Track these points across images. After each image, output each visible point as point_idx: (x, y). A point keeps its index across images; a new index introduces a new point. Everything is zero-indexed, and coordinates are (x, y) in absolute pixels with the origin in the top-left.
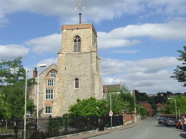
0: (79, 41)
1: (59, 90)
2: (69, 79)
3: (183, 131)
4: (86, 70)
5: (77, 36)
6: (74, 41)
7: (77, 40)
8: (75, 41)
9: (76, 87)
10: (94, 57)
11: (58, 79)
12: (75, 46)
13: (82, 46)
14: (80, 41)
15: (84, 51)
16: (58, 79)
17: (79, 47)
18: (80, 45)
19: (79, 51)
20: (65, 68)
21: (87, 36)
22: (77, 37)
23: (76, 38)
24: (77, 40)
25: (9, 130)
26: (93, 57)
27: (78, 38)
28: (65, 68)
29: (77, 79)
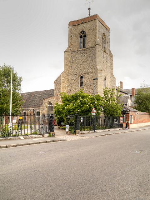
0: (85, 36)
1: (64, 89)
2: (74, 78)
3: (49, 137)
4: (91, 66)
5: (82, 31)
6: (80, 38)
7: (83, 35)
8: (81, 37)
9: (81, 86)
10: (99, 51)
11: (63, 78)
12: (81, 43)
13: (87, 41)
14: (86, 36)
15: (89, 46)
16: (63, 78)
17: (85, 43)
18: (85, 40)
19: (85, 47)
20: (71, 66)
21: (92, 29)
22: (83, 32)
23: (82, 34)
24: (83, 35)
25: (25, 132)
26: (97, 51)
27: (84, 33)
28: (71, 66)
29: (82, 78)
